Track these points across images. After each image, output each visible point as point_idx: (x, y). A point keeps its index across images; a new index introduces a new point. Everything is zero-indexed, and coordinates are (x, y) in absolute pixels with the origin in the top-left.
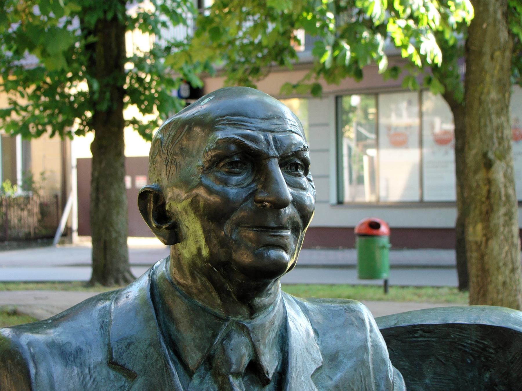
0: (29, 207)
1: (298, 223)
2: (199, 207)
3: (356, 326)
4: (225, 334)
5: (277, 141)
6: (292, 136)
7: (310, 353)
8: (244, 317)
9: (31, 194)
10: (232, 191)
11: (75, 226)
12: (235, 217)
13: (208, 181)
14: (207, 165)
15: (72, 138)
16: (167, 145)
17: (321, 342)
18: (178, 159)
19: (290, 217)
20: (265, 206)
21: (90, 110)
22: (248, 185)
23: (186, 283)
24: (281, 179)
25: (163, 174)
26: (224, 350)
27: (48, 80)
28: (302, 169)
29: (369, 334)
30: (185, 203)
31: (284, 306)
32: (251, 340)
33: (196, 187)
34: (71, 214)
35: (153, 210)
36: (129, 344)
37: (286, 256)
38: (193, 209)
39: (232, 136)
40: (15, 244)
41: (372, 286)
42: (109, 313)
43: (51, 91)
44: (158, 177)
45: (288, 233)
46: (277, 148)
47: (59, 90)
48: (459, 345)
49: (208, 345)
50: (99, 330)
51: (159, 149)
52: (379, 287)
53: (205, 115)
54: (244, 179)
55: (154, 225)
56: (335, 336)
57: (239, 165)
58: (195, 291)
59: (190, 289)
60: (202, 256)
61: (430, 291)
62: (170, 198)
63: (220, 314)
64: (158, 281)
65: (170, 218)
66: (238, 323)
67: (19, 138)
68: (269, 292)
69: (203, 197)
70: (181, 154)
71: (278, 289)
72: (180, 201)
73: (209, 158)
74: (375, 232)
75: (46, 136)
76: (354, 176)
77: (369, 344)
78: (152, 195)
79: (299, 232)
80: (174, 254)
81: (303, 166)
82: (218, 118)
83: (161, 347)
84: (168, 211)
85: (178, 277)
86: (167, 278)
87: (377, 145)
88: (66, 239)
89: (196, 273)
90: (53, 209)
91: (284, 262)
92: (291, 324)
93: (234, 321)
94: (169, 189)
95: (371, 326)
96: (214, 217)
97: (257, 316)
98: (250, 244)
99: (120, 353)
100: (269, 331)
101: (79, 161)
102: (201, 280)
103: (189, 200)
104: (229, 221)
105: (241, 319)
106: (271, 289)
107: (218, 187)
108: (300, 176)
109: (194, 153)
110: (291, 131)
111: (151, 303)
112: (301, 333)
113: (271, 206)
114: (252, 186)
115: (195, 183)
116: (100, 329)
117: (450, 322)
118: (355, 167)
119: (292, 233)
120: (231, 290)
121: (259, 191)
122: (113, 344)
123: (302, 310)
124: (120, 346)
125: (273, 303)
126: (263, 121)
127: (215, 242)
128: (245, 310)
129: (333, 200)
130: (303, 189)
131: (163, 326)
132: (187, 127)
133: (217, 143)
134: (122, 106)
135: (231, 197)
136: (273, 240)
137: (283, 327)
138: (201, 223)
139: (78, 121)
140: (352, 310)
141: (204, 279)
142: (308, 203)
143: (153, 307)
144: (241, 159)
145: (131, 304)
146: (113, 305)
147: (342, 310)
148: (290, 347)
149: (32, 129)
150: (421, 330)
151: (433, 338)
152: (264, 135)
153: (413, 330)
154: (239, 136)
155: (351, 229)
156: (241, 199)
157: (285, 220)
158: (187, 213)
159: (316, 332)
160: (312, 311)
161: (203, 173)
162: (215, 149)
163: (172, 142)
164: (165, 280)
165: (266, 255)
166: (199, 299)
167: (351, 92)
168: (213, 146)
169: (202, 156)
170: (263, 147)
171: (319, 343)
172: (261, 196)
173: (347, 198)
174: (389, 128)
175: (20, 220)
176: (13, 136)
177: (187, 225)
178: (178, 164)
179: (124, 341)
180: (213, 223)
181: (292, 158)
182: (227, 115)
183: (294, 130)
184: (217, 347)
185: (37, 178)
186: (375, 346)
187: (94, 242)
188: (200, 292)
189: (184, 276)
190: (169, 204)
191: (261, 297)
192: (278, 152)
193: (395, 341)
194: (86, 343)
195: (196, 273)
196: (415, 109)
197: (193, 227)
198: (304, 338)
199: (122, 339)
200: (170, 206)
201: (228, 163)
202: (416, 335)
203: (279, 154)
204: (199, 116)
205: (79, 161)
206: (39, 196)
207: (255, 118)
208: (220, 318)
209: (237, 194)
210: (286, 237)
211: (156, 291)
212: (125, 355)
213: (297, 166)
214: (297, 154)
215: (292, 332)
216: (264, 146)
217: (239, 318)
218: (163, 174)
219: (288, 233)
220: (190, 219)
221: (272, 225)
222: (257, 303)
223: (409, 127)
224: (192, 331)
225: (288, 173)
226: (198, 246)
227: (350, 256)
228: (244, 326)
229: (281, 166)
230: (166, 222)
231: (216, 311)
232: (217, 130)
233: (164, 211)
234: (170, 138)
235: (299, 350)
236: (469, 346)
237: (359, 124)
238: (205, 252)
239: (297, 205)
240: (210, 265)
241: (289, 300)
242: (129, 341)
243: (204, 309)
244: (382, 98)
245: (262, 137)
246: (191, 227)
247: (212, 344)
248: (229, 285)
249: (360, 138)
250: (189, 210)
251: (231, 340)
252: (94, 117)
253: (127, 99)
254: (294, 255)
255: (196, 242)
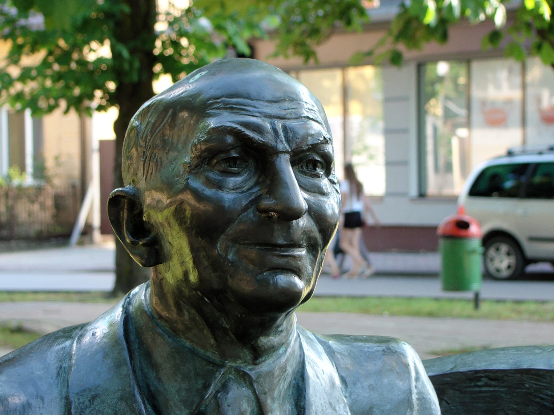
0: (41, 199)
1: (315, 239)
2: (184, 217)
3: (397, 373)
4: (220, 385)
6: (309, 124)
7: (334, 409)
8: (245, 362)
9: (42, 183)
10: (228, 197)
11: (96, 221)
12: (231, 230)
13: (197, 184)
14: (195, 162)
15: (91, 115)
17: (350, 393)
18: (160, 154)
19: (304, 231)
20: (271, 217)
21: (113, 80)
22: (249, 189)
23: (170, 316)
25: (140, 173)
26: (218, 406)
27: (62, 43)
28: (322, 168)
29: (414, 384)
30: (167, 212)
32: (254, 392)
33: (182, 191)
34: (92, 208)
36: (94, 398)
38: (177, 221)
39: (228, 124)
40: (23, 244)
41: (460, 300)
42: (70, 355)
43: (64, 58)
44: (133, 178)
45: (303, 252)
46: (288, 141)
47: (75, 56)
48: (536, 397)
49: (197, 400)
50: (54, 378)
51: (135, 140)
52: (468, 301)
53: (194, 96)
54: (245, 181)
56: (369, 386)
57: (238, 162)
58: (180, 327)
59: (175, 325)
60: (190, 281)
61: (533, 307)
62: (149, 205)
63: (214, 358)
64: (134, 314)
65: (149, 232)
66: (238, 371)
67: (28, 113)
68: (280, 329)
69: (190, 205)
70: (164, 148)
71: (292, 325)
72: (161, 210)
73: (197, 153)
74: (462, 232)
75: (58, 113)
76: (441, 162)
77: (414, 397)
78: (126, 201)
79: (317, 251)
81: (324, 164)
84: (146, 222)
86: (146, 309)
87: (468, 124)
88: (86, 239)
89: (182, 303)
90: (69, 202)
91: (297, 290)
92: (309, 370)
93: (231, 367)
94: (147, 193)
95: (417, 373)
96: (205, 229)
98: (251, 267)
99: (82, 409)
100: (279, 380)
102: (190, 314)
103: (173, 208)
104: (223, 236)
105: (242, 365)
106: (281, 324)
107: (209, 192)
108: (319, 177)
109: (180, 146)
110: (308, 118)
112: (323, 382)
113: (279, 217)
114: (255, 190)
115: (179, 186)
116: (57, 377)
117: (525, 367)
118: (442, 152)
119: (308, 252)
120: (227, 326)
121: (263, 196)
122: (72, 397)
123: (326, 352)
124: (81, 400)
125: (284, 344)
126: (269, 105)
128: (247, 353)
129: (414, 191)
130: (323, 194)
131: (139, 373)
132: (171, 112)
133: (209, 133)
134: (152, 76)
135: (227, 205)
137: (299, 374)
139: (98, 93)
140: (392, 352)
141: (193, 311)
142: (330, 212)
146: (75, 345)
147: (379, 351)
148: (307, 402)
149: (42, 104)
150: (486, 376)
151: (502, 387)
152: (271, 123)
153: (475, 376)
154: (238, 124)
155: (433, 229)
156: (239, 208)
157: (298, 235)
158: (169, 224)
159: (343, 380)
160: (340, 353)
161: (190, 172)
162: (206, 141)
163: (151, 131)
164: (143, 312)
165: (272, 282)
166: (187, 339)
167: (436, 59)
168: (202, 136)
170: (269, 139)
172: (267, 203)
173: (432, 188)
174: (484, 103)
175: (30, 214)
176: (21, 112)
177: (171, 241)
178: (159, 160)
179: (87, 393)
180: (203, 239)
181: (308, 153)
182: (222, 97)
183: (311, 117)
185: (50, 163)
186: (423, 399)
188: (188, 329)
189: (166, 306)
190: (147, 213)
191: (267, 335)
192: (289, 145)
193: (452, 391)
194: (37, 396)
195: (182, 303)
196: (517, 80)
197: (177, 242)
199: (85, 390)
200: (149, 215)
201: (223, 160)
202: (479, 384)
203: (291, 148)
205: (102, 143)
206: (52, 186)
207: (260, 100)
208: (214, 364)
209: (234, 200)
210: (299, 258)
211: (131, 327)
212: (87, 411)
213: (315, 164)
214: (315, 148)
215: (311, 381)
216: (270, 137)
217: (239, 363)
218: (140, 173)
219: (303, 252)
220: (174, 233)
221: (281, 241)
223: (509, 102)
224: (176, 381)
225: (304, 173)
226: (184, 269)
227: (433, 261)
228: (245, 374)
229: (293, 164)
230: (144, 236)
231: (209, 354)
232: (210, 116)
233: (142, 222)
235: (320, 405)
236: (550, 398)
237: (447, 98)
238: (193, 277)
240: (200, 294)
242: (93, 393)
243: (193, 352)
244: (476, 66)
245: (269, 126)
246: (175, 244)
249: (448, 115)
250: (173, 221)
251: (227, 393)
252: (118, 89)
253: (158, 68)
254: (310, 282)
255: (183, 263)
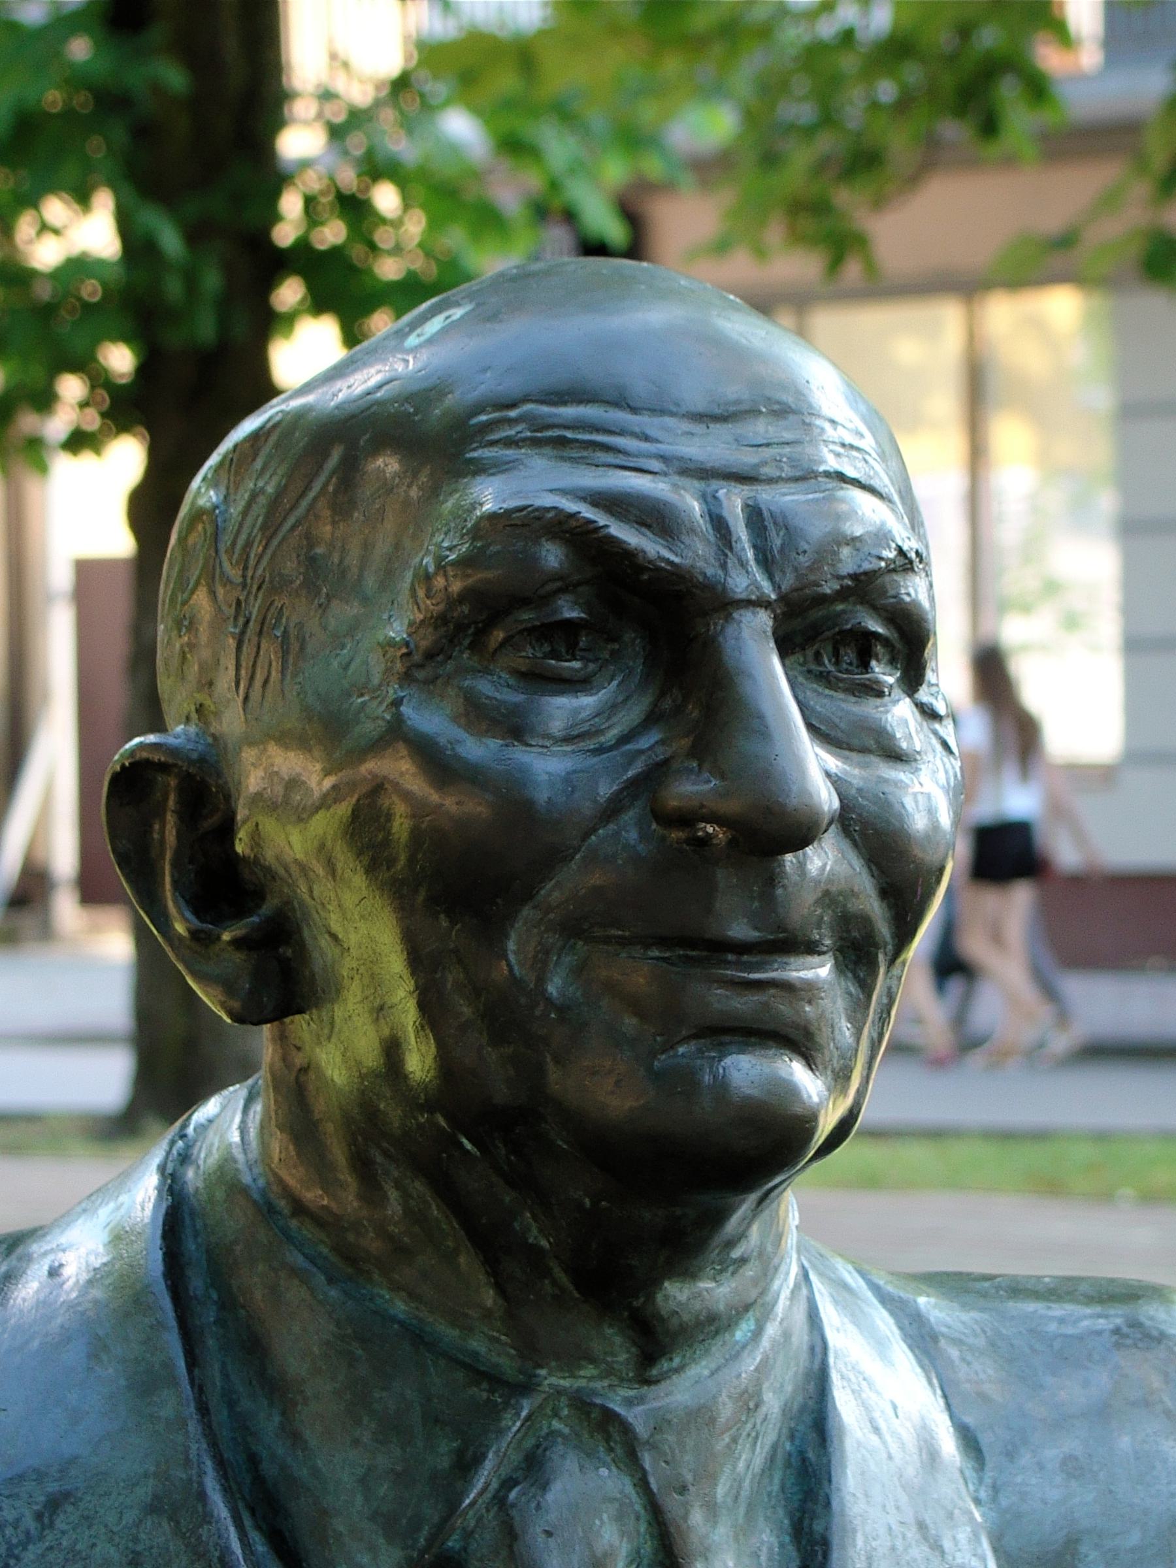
1: (865, 921)
2: (386, 843)
4: (516, 1457)
5: (769, 523)
6: (843, 500)
8: (609, 1372)
10: (546, 768)
11: (64, 857)
12: (560, 889)
14: (426, 640)
15: (42, 468)
16: (240, 542)
17: (995, 1489)
19: (827, 893)
20: (705, 842)
22: (624, 739)
24: (781, 708)
25: (225, 680)
26: (510, 1534)
28: (892, 662)
30: (325, 824)
31: (814, 1318)
32: (643, 1484)
35: (178, 853)
36: (54, 1504)
37: (807, 1082)
39: (549, 501)
44: (200, 697)
45: (820, 970)
46: (766, 561)
49: (432, 1513)
53: (423, 396)
54: (611, 709)
55: (180, 928)
57: (583, 641)
58: (372, 1243)
59: (351, 1237)
60: (406, 1077)
62: (257, 798)
65: (259, 895)
66: (582, 1404)
68: (736, 1254)
69: (407, 796)
70: (310, 587)
71: (779, 1237)
72: (302, 815)
73: (433, 606)
78: (173, 782)
80: (279, 1064)
81: (899, 646)
82: (482, 411)
83: (207, 1517)
84: (244, 859)
85: (293, 1178)
86: (246, 1179)
88: (27, 921)
89: (379, 1159)
91: (798, 1110)
92: (843, 1401)
93: (560, 1392)
94: (249, 755)
96: (463, 884)
97: (678, 1370)
98: (630, 1023)
99: (10, 1547)
100: (735, 1440)
101: (86, 571)
102: (406, 1195)
103: (343, 809)
105: (598, 1385)
106: (742, 1236)
107: (477, 749)
108: (880, 694)
109: (370, 582)
110: (841, 477)
111: (167, 1303)
112: (894, 1448)
113: (732, 843)
114: (644, 742)
115: (369, 728)
120: (544, 1243)
123: (907, 1337)
125: (754, 1306)
126: (699, 428)
127: (467, 1011)
128: (618, 1340)
130: (896, 756)
131: (220, 1415)
133: (476, 533)
134: (268, 323)
135: (542, 796)
136: (742, 1004)
137: (808, 1419)
138: (400, 920)
139: (72, 387)
140: (1147, 1336)
141: (419, 1187)
142: (919, 823)
143: (172, 1323)
144: (590, 614)
145: (71, 1306)
147: (1099, 1333)
148: (836, 1520)
152: (704, 497)
154: (584, 499)
156: (587, 809)
159: (969, 1440)
160: (958, 1342)
161: (407, 678)
162: (465, 563)
163: (264, 528)
165: (707, 1078)
166: (396, 1287)
169: (404, 596)
170: (696, 554)
171: (983, 1494)
172: (690, 788)
177: (336, 927)
178: (293, 632)
180: (453, 923)
181: (840, 607)
182: (526, 399)
183: (851, 473)
184: (480, 1520)
187: (142, 937)
188: (401, 1251)
189: (321, 1170)
191: (690, 1275)
192: (771, 578)
195: (379, 1159)
197: (362, 936)
198: (910, 1471)
199: (21, 1477)
200: (256, 837)
201: (530, 631)
203: (776, 587)
204: (394, 400)
205: (86, 571)
207: (663, 412)
208: (494, 1379)
210: (809, 991)
211: (191, 1246)
214: (866, 587)
215: (849, 1444)
216: (701, 548)
217: (585, 1379)
218: (225, 680)
219: (820, 970)
220: (349, 899)
221: (740, 930)
222: (672, 1305)
224: (356, 1442)
225: (824, 678)
226: (386, 1032)
230: (240, 913)
231: (477, 1344)
232: (480, 469)
233: (233, 860)
234: (259, 509)
235: (882, 1531)
238: (419, 1062)
239: (863, 833)
240: (442, 1122)
241: (845, 1286)
242: (53, 1487)
245: (696, 507)
247: (452, 1506)
248: (535, 1217)
250: (344, 858)
251: (545, 1487)
252: (144, 370)
253: (289, 293)
254: (848, 1078)
255: (380, 1011)
